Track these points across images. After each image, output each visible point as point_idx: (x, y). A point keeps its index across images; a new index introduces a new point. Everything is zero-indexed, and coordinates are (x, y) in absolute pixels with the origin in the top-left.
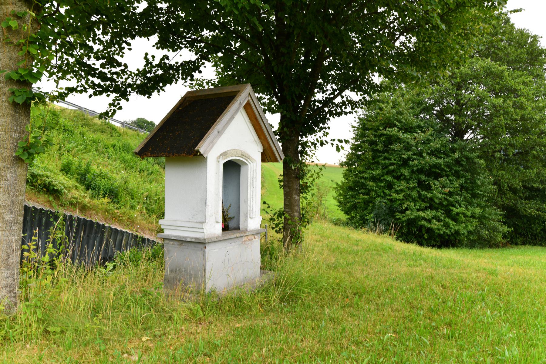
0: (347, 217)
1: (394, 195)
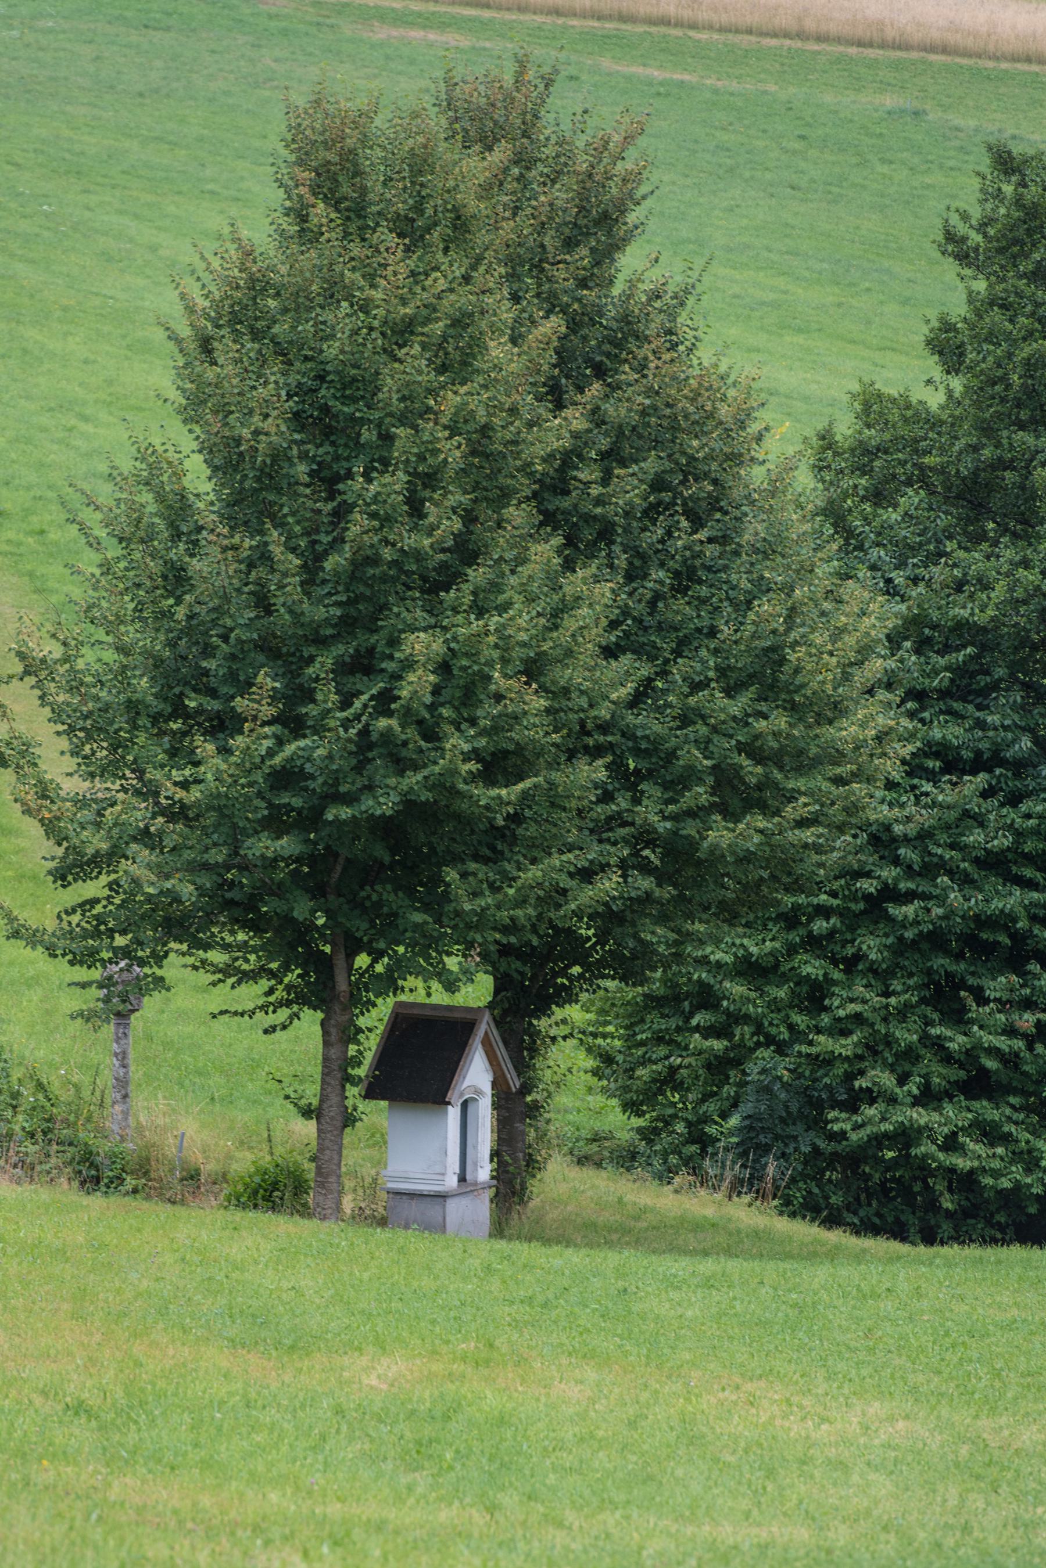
0: (637, 1122)
1: (824, 1043)
